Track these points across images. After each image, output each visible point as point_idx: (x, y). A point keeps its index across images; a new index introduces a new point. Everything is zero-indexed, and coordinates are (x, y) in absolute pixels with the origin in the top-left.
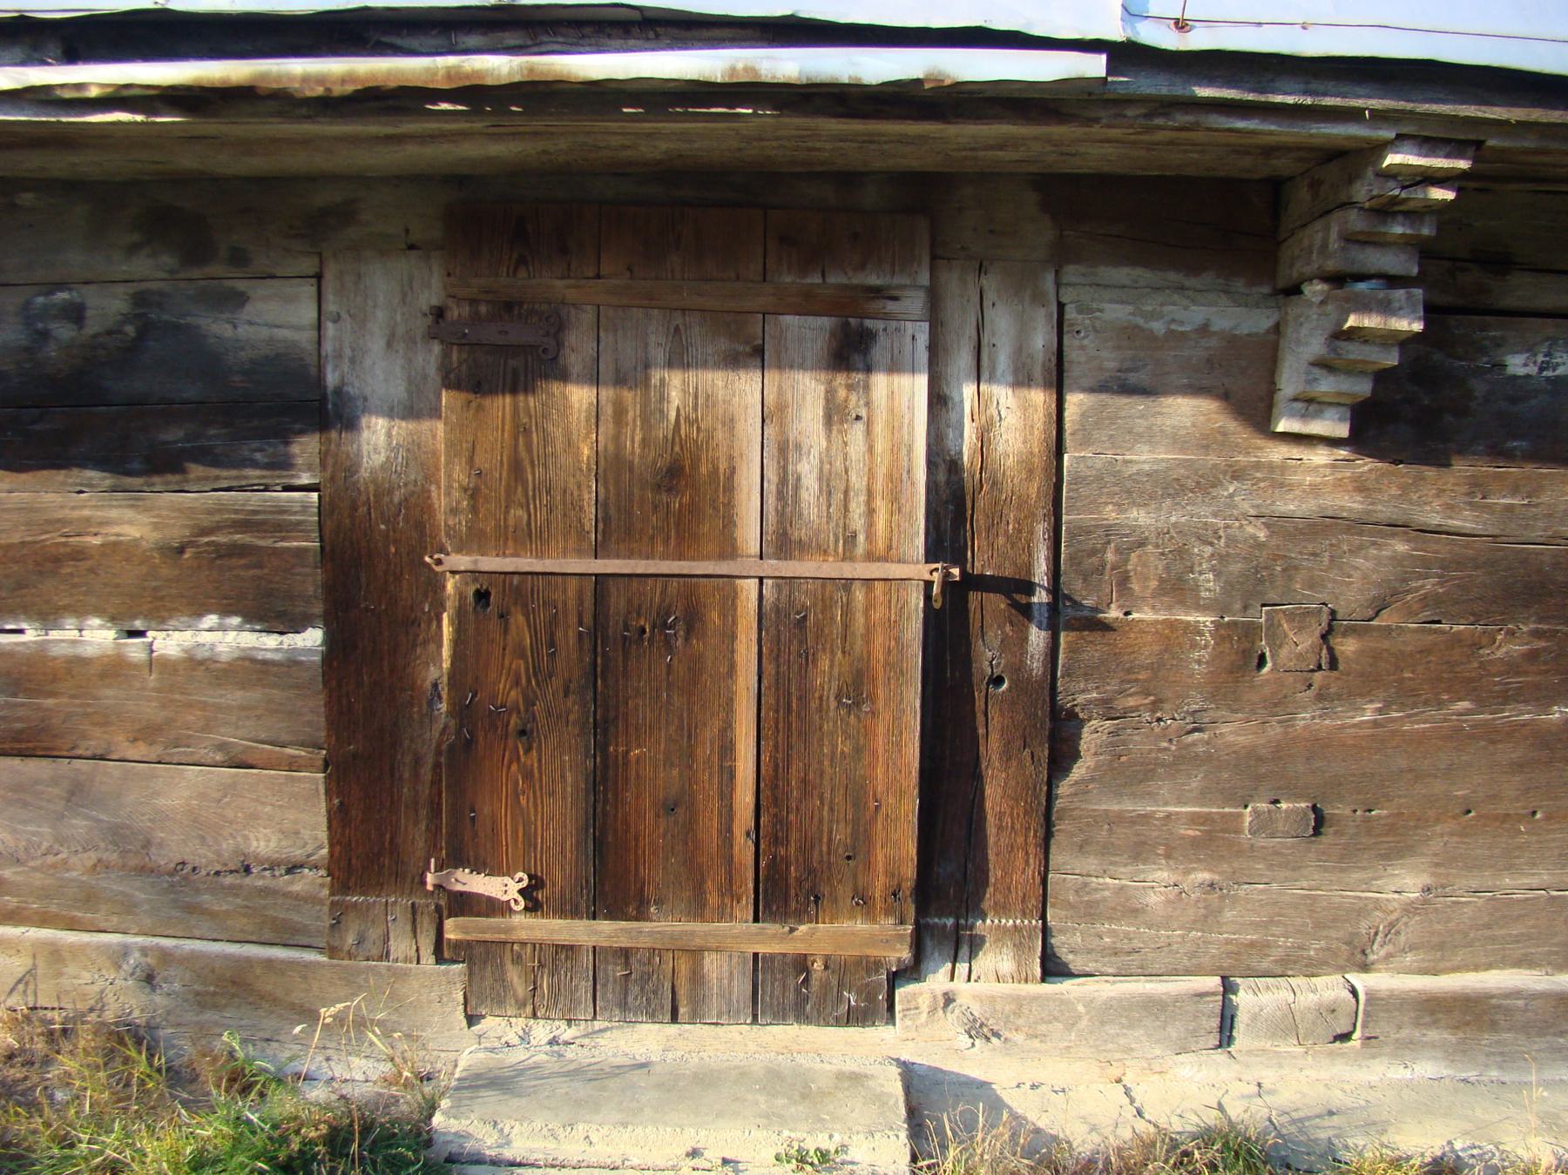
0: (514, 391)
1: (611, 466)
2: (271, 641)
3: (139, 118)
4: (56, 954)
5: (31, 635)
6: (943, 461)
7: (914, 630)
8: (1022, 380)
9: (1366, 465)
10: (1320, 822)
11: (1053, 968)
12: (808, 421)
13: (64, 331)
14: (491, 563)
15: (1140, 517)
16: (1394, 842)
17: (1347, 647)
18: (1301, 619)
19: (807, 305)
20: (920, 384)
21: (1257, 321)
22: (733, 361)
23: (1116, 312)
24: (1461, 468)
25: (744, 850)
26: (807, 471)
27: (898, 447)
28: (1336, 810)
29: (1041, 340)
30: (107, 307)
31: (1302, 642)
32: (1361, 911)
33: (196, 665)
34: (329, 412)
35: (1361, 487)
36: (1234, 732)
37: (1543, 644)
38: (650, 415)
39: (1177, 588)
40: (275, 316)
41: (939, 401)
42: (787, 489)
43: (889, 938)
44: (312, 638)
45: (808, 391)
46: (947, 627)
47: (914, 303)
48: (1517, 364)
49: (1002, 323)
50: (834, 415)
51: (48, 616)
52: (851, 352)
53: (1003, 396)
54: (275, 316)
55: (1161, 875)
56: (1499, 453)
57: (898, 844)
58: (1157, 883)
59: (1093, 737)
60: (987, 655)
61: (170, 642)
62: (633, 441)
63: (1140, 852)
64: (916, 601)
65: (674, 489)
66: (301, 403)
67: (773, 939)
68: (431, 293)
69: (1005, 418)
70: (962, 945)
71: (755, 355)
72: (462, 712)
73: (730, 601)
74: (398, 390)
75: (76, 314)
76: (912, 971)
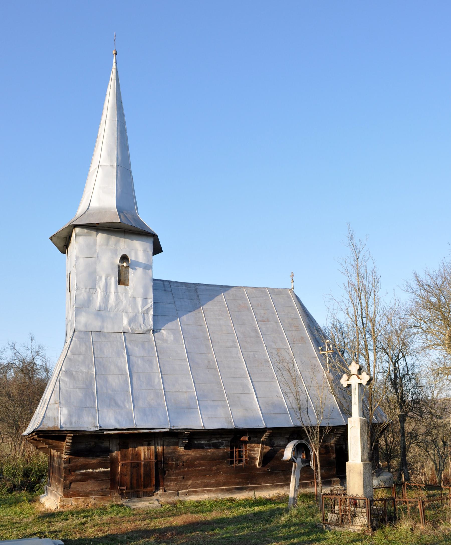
0: (125, 449)
1: (132, 454)
2: (105, 470)
3: (97, 471)
4: (86, 498)
5: (85, 471)
6: (156, 452)
7: (154, 465)
8: (161, 446)
9: (185, 450)
10: (184, 478)
11: (165, 491)
12: (146, 450)
13: (89, 446)
14: (123, 462)
15: (169, 455)
16: (189, 479)
17: (185, 464)
18: (181, 462)
19: (146, 441)
20: (154, 447)
21: (177, 440)
22: (141, 446)
23: (167, 440)
24: (193, 450)
25: (142, 483)
26: (146, 454)
27: (153, 451)
28: (185, 477)
29: (162, 443)
30: (92, 444)
31: (181, 464)
32: (187, 485)
33: (99, 472)
34: (112, 452)
35: (185, 452)
36: (177, 471)
37: (403, 475)
38: (135, 450)
39: (172, 461)
40: (106, 444)
41: (155, 448)
42: (145, 455)
43: (152, 488)
44: (109, 469)
45: (146, 448)
46: (156, 464)
47: (153, 441)
48: (195, 442)
49: (159, 442)
50: (148, 449)
51: (86, 469)
52: (149, 445)
53: (160, 447)
54: (106, 444)
55: (172, 483)
56: (194, 448)
57: (154, 482)
58: (172, 484)
59: (167, 472)
60: (159, 467)
61: (97, 471)
62: (134, 452)
63: (171, 481)
64: (154, 463)
65: (137, 455)
66: (108, 451)
67: (145, 490)
68: (118, 442)
69: (160, 448)
70: (158, 489)
71: (142, 445)
72: (121, 474)
73: (141, 464)
74: (116, 449)
75: (90, 444)
76: (155, 492)
